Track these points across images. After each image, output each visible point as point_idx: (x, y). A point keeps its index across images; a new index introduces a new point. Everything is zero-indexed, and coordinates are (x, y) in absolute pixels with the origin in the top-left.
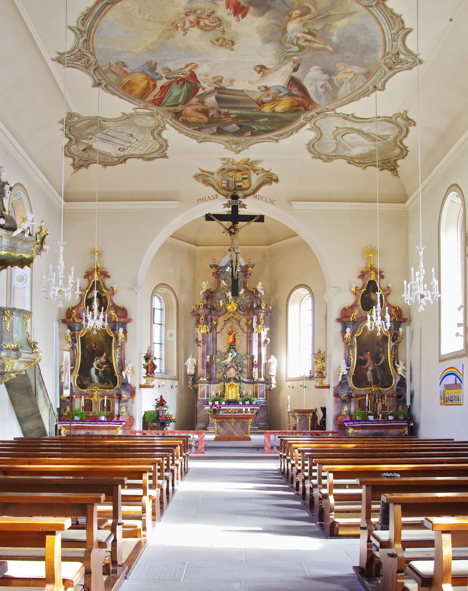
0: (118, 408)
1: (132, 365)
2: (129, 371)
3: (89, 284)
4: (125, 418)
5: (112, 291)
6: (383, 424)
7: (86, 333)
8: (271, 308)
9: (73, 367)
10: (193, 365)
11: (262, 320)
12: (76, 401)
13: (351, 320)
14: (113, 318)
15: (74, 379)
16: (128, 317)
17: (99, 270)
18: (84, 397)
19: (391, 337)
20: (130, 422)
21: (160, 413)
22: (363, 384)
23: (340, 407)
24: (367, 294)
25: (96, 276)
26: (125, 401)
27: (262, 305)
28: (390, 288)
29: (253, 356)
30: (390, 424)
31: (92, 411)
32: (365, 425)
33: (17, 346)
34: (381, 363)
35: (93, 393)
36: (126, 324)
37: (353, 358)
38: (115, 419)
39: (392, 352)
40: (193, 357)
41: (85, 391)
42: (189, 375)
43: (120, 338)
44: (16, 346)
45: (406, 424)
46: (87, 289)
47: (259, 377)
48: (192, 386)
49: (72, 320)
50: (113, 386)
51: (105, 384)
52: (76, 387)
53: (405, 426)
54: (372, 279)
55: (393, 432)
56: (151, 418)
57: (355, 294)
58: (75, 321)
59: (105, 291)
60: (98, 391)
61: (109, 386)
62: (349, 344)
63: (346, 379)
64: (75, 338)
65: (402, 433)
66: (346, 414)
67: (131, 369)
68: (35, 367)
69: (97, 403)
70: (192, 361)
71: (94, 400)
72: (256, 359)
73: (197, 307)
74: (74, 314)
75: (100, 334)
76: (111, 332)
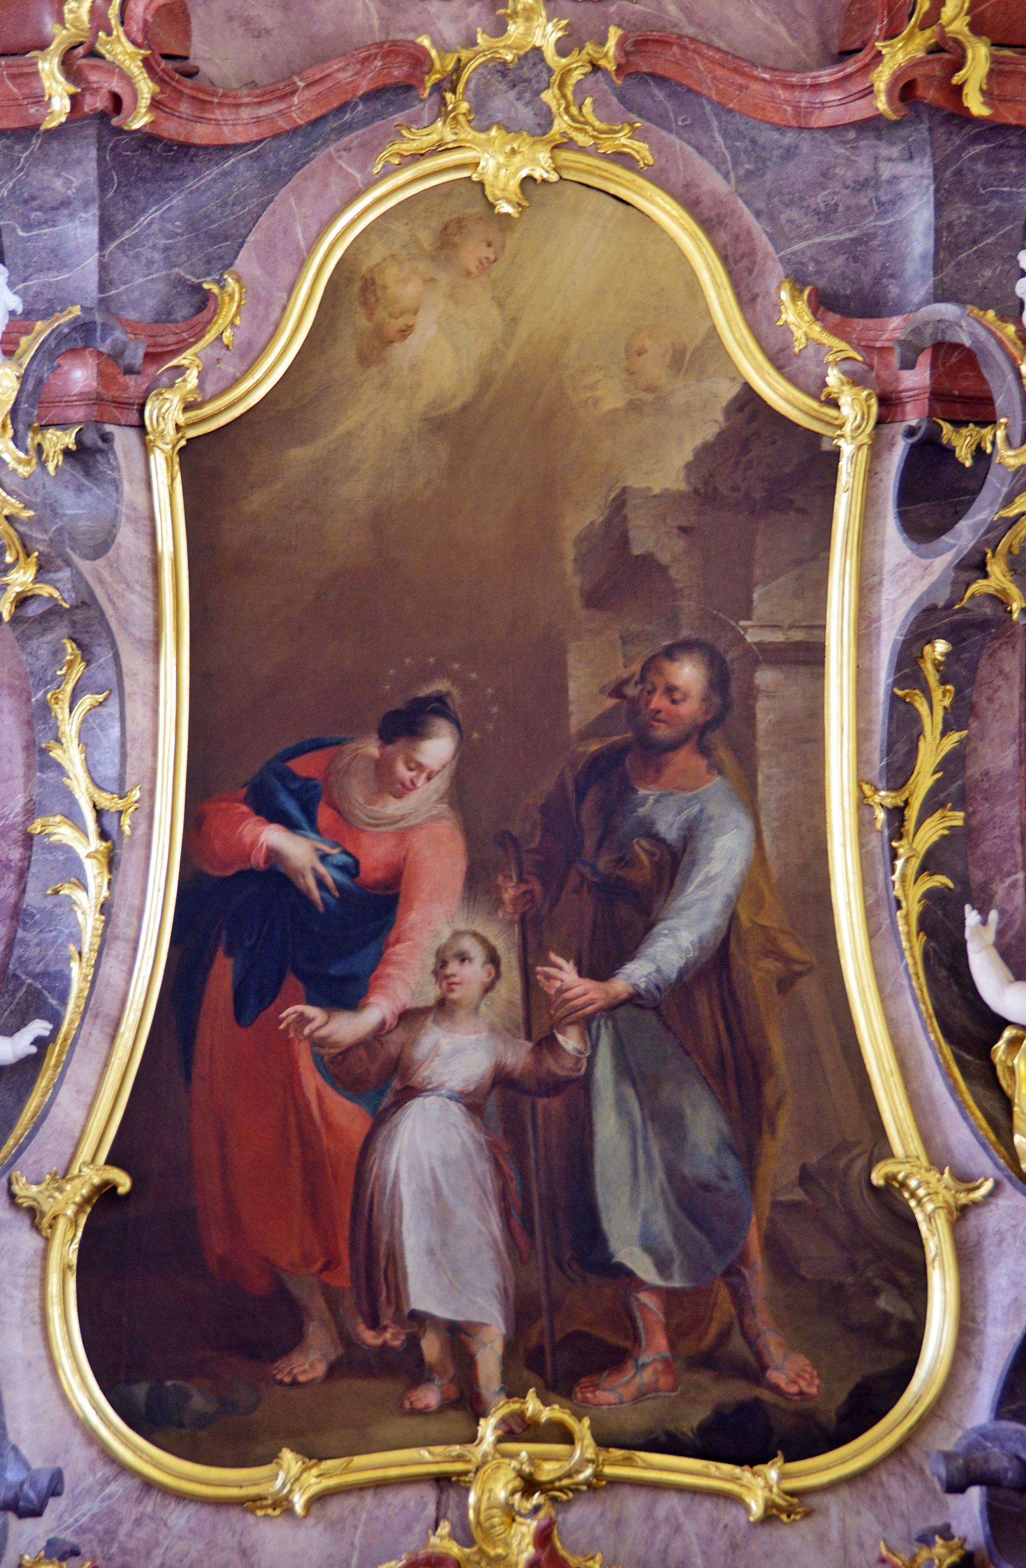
13: (60, 106)
19: (876, 450)
37: (112, 862)
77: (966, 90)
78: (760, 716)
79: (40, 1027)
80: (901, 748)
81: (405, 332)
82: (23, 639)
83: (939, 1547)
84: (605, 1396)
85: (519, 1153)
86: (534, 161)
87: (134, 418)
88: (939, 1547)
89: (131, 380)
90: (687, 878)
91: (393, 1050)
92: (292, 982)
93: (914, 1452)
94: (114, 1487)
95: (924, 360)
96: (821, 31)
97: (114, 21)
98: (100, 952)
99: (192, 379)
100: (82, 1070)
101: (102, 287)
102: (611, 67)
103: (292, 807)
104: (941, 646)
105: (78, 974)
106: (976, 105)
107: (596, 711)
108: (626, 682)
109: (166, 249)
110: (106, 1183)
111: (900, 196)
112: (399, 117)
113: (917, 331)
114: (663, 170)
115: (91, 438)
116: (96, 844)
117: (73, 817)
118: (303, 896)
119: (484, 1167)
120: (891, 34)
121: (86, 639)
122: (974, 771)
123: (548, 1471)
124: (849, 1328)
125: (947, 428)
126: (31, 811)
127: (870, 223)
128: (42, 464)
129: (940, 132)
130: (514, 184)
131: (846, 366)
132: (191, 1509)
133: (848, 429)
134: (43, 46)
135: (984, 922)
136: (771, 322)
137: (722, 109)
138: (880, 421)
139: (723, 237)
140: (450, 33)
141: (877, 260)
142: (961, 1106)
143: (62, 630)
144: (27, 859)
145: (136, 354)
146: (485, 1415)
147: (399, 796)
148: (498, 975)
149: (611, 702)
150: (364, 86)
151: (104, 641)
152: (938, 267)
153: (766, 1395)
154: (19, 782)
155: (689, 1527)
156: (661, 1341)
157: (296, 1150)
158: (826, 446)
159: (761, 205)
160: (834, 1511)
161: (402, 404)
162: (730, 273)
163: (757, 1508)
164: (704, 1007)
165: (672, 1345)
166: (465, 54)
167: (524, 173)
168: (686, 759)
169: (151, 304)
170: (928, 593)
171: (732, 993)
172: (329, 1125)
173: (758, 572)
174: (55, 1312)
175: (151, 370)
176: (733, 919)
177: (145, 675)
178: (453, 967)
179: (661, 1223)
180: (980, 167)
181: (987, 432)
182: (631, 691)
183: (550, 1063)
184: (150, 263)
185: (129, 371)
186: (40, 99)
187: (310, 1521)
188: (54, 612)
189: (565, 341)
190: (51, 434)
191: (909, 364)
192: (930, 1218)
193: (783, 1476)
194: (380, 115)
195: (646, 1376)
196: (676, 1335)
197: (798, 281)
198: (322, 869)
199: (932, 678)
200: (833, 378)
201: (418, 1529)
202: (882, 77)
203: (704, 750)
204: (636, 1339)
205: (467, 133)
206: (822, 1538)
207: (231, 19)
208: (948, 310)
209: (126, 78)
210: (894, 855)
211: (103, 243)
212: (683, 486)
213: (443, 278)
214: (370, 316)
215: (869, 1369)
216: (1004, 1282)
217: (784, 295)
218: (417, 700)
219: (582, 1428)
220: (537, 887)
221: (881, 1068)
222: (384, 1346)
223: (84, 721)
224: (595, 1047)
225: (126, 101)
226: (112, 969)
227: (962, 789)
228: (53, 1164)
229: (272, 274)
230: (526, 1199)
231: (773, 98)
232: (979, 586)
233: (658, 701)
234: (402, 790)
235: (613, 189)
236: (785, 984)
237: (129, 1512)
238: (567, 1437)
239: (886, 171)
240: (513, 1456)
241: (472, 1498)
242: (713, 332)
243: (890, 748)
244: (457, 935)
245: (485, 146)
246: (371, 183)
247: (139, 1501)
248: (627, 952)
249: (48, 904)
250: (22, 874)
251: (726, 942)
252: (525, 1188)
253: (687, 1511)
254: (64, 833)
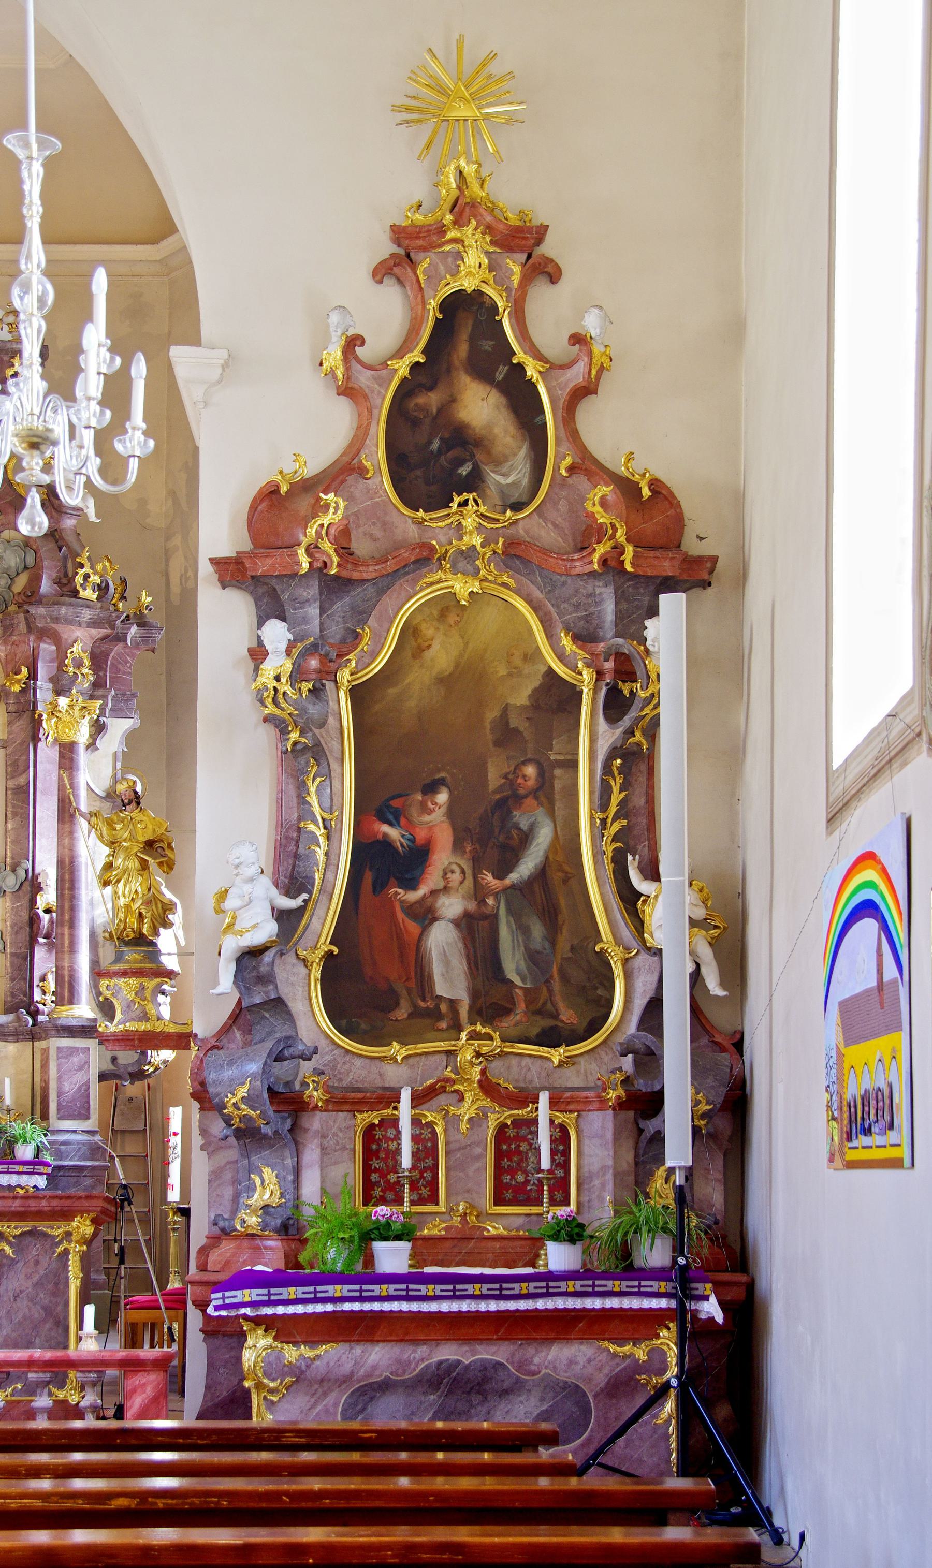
6: (493, 1306)
8: (146, 599)
11: (79, 664)
13: (305, 566)
19: (596, 691)
22: (402, 1013)
23: (228, 1175)
24: (431, 389)
27: (79, 579)
28: (597, 349)
29: (35, 877)
30: (541, 1304)
32: (357, 1306)
34: (526, 868)
37: (328, 838)
39: (606, 792)
45: (663, 1303)
46: (399, 354)
47: (59, 1002)
53: (655, 1319)
54: (469, 284)
55: (571, 1362)
57: (347, 391)
62: (294, 736)
63: (267, 979)
65: (637, 1368)
66: (264, 1226)
72: (48, 897)
77: (626, 562)
78: (556, 786)
79: (305, 896)
80: (605, 797)
81: (429, 647)
82: (295, 758)
83: (618, 1075)
84: (504, 1024)
85: (473, 941)
86: (474, 586)
87: (333, 678)
88: (618, 1075)
89: (332, 664)
90: (531, 844)
91: (429, 904)
92: (393, 880)
93: (609, 1042)
94: (335, 1052)
95: (612, 658)
96: (574, 540)
97: (324, 536)
98: (325, 870)
99: (353, 664)
100: (320, 911)
101: (321, 631)
102: (500, 552)
103: (391, 818)
104: (619, 761)
105: (318, 877)
106: (629, 568)
107: (499, 784)
108: (508, 773)
109: (344, 617)
110: (330, 950)
111: (603, 600)
112: (425, 570)
113: (609, 648)
114: (519, 589)
115: (318, 685)
116: (323, 831)
117: (315, 822)
118: (396, 850)
119: (461, 945)
120: (599, 542)
121: (317, 758)
122: (630, 806)
123: (485, 1050)
124: (588, 1001)
125: (620, 683)
126: (300, 819)
127: (592, 609)
128: (301, 695)
129: (616, 578)
130: (466, 594)
131: (585, 660)
132: (362, 1059)
133: (585, 683)
134: (299, 545)
135: (634, 859)
136: (558, 644)
137: (539, 567)
138: (597, 680)
139: (541, 613)
140: (443, 539)
141: (595, 622)
142: (626, 923)
143: (309, 754)
144: (299, 836)
145: (333, 655)
146: (462, 1031)
147: (429, 814)
148: (465, 878)
149: (503, 781)
150: (413, 558)
151: (324, 758)
152: (616, 625)
153: (559, 1024)
154: (295, 809)
155: (533, 1069)
156: (523, 1005)
157: (395, 939)
158: (578, 689)
159: (553, 602)
160: (582, 1063)
161: (428, 673)
162: (543, 627)
163: (556, 1062)
164: (537, 888)
165: (527, 1007)
166: (448, 547)
167: (470, 590)
168: (530, 801)
169: (338, 637)
170: (614, 742)
171: (547, 884)
172: (407, 931)
173: (554, 734)
174: (313, 995)
175: (339, 661)
176: (547, 858)
177: (338, 770)
178: (449, 875)
179: (523, 965)
180: (630, 590)
181: (634, 685)
182: (510, 777)
183: (483, 909)
184: (338, 622)
185: (331, 661)
186: (298, 564)
187: (403, 1065)
188: (306, 748)
189: (485, 650)
190: (304, 684)
191: (607, 660)
192: (615, 962)
193: (565, 1051)
194: (419, 569)
195: (518, 1018)
196: (529, 1003)
197: (567, 630)
198: (402, 840)
199: (616, 773)
200: (580, 664)
201: (440, 1069)
202: (596, 557)
203: (536, 798)
204: (515, 1004)
205: (450, 576)
206: (578, 1072)
207: (365, 534)
208: (620, 641)
209: (329, 556)
210: (603, 836)
211: (321, 616)
212: (528, 703)
213: (442, 627)
214: (416, 641)
215: (594, 1015)
216: (641, 984)
217: (563, 635)
218: (435, 780)
219: (496, 1035)
220: (477, 846)
221: (599, 910)
222: (427, 1007)
223: (318, 787)
224: (499, 903)
225: (329, 564)
226: (330, 876)
227: (626, 812)
228: (311, 944)
229: (381, 626)
230: (476, 957)
231: (558, 564)
232: (632, 740)
233: (520, 780)
234: (430, 812)
235: (501, 596)
236: (565, 881)
237: (341, 1060)
238: (491, 1039)
239: (598, 591)
240: (472, 1045)
241: (459, 1059)
242: (538, 648)
243: (601, 798)
244: (450, 864)
245: (456, 580)
246: (416, 594)
247: (344, 1056)
248: (510, 871)
249: (307, 852)
250: (297, 842)
251: (544, 866)
252: (475, 952)
253: (532, 1063)
254: (312, 827)
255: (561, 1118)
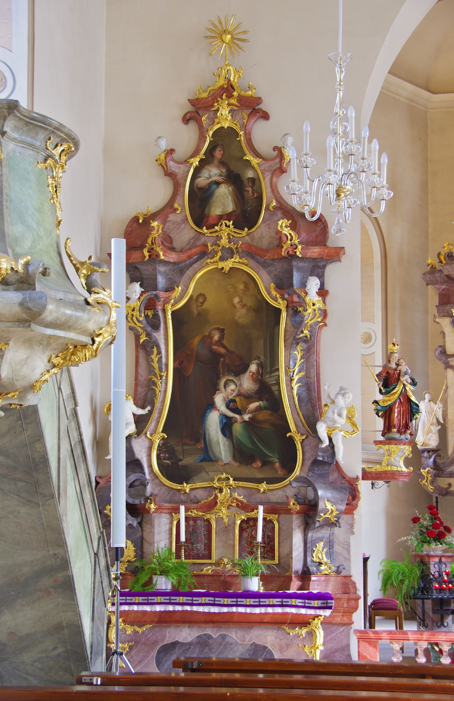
0: (301, 549)
1: (348, 400)
2: (342, 421)
3: (202, 138)
4: (327, 581)
5: (278, 160)
7: (191, 297)
9: (149, 408)
10: (435, 420)
12: (156, 522)
14: (285, 247)
15: (150, 449)
16: (330, 243)
17: (235, 94)
18: (187, 510)
20: (349, 600)
21: (432, 567)
25: (224, 111)
26: (330, 524)
31: (210, 558)
33: (27, 264)
35: (216, 497)
36: (324, 267)
38: (294, 589)
40: (433, 400)
41: (187, 487)
42: (423, 451)
43: (310, 311)
44: (20, 268)
46: (193, 155)
48: (432, 483)
49: (147, 254)
50: (280, 473)
51: (254, 465)
52: (156, 477)
56: (402, 582)
58: (158, 256)
59: (255, 161)
60: (233, 490)
61: (268, 474)
64: (156, 316)
67: (345, 413)
68: (59, 389)
69: (228, 529)
70: (430, 412)
71: (219, 520)
73: (442, 258)
74: (155, 234)
75: (236, 300)
76: (274, 293)
255: (271, 517)
